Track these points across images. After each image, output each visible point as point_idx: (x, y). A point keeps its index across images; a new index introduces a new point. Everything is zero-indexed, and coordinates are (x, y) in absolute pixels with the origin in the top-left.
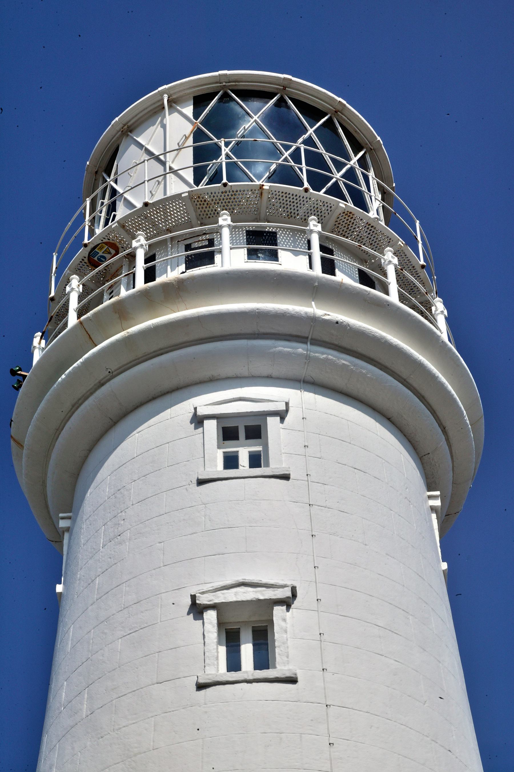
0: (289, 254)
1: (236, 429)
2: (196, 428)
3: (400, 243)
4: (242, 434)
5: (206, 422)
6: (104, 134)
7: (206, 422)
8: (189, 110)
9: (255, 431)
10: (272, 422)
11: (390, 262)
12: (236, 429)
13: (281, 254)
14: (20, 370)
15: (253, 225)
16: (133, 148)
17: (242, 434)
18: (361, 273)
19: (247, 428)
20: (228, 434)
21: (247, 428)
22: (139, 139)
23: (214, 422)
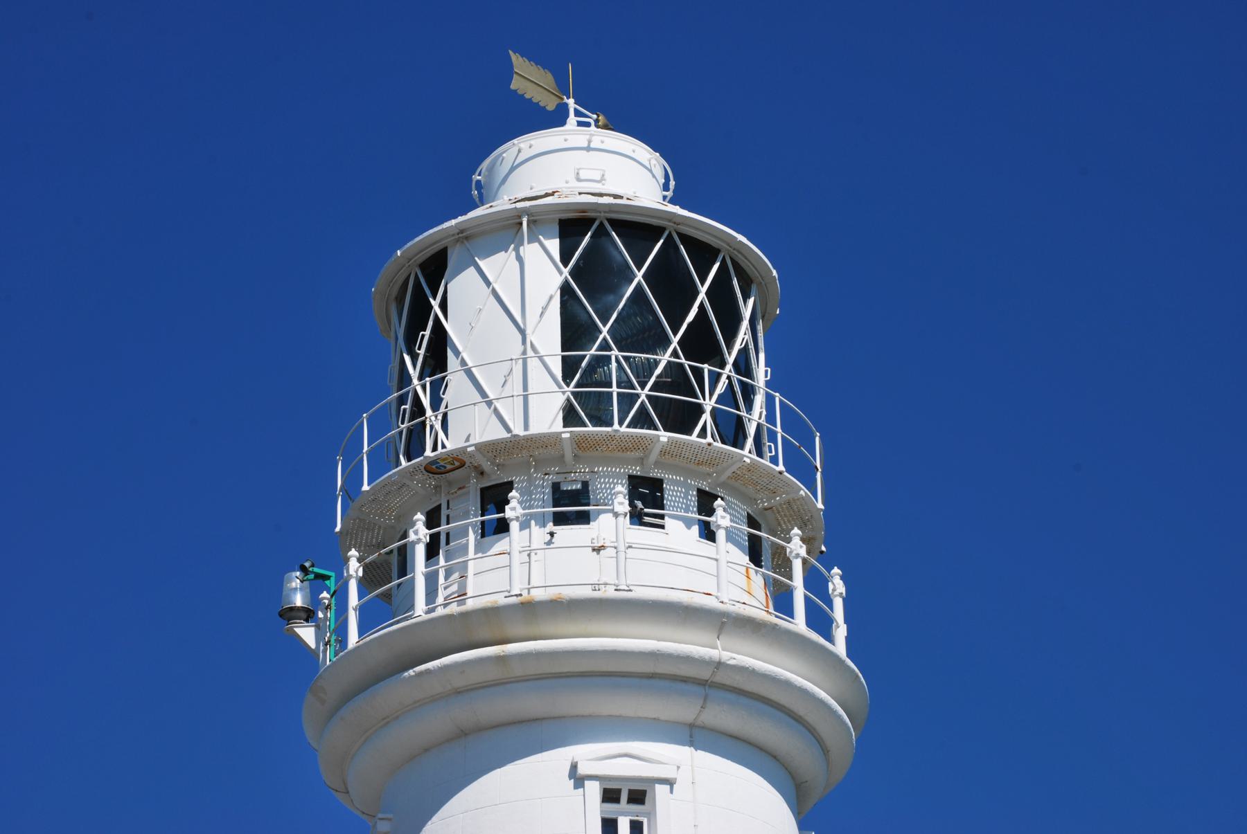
0: (680, 524)
1: (619, 791)
2: (576, 787)
3: (802, 492)
4: (624, 797)
5: (587, 783)
6: (431, 231)
7: (587, 783)
8: (554, 245)
9: (638, 797)
10: (661, 790)
11: (797, 556)
12: (619, 791)
13: (668, 521)
14: (313, 566)
15: (637, 471)
16: (471, 270)
17: (624, 797)
18: (749, 517)
19: (631, 792)
20: (610, 796)
21: (631, 792)
22: (481, 263)
23: (597, 783)
